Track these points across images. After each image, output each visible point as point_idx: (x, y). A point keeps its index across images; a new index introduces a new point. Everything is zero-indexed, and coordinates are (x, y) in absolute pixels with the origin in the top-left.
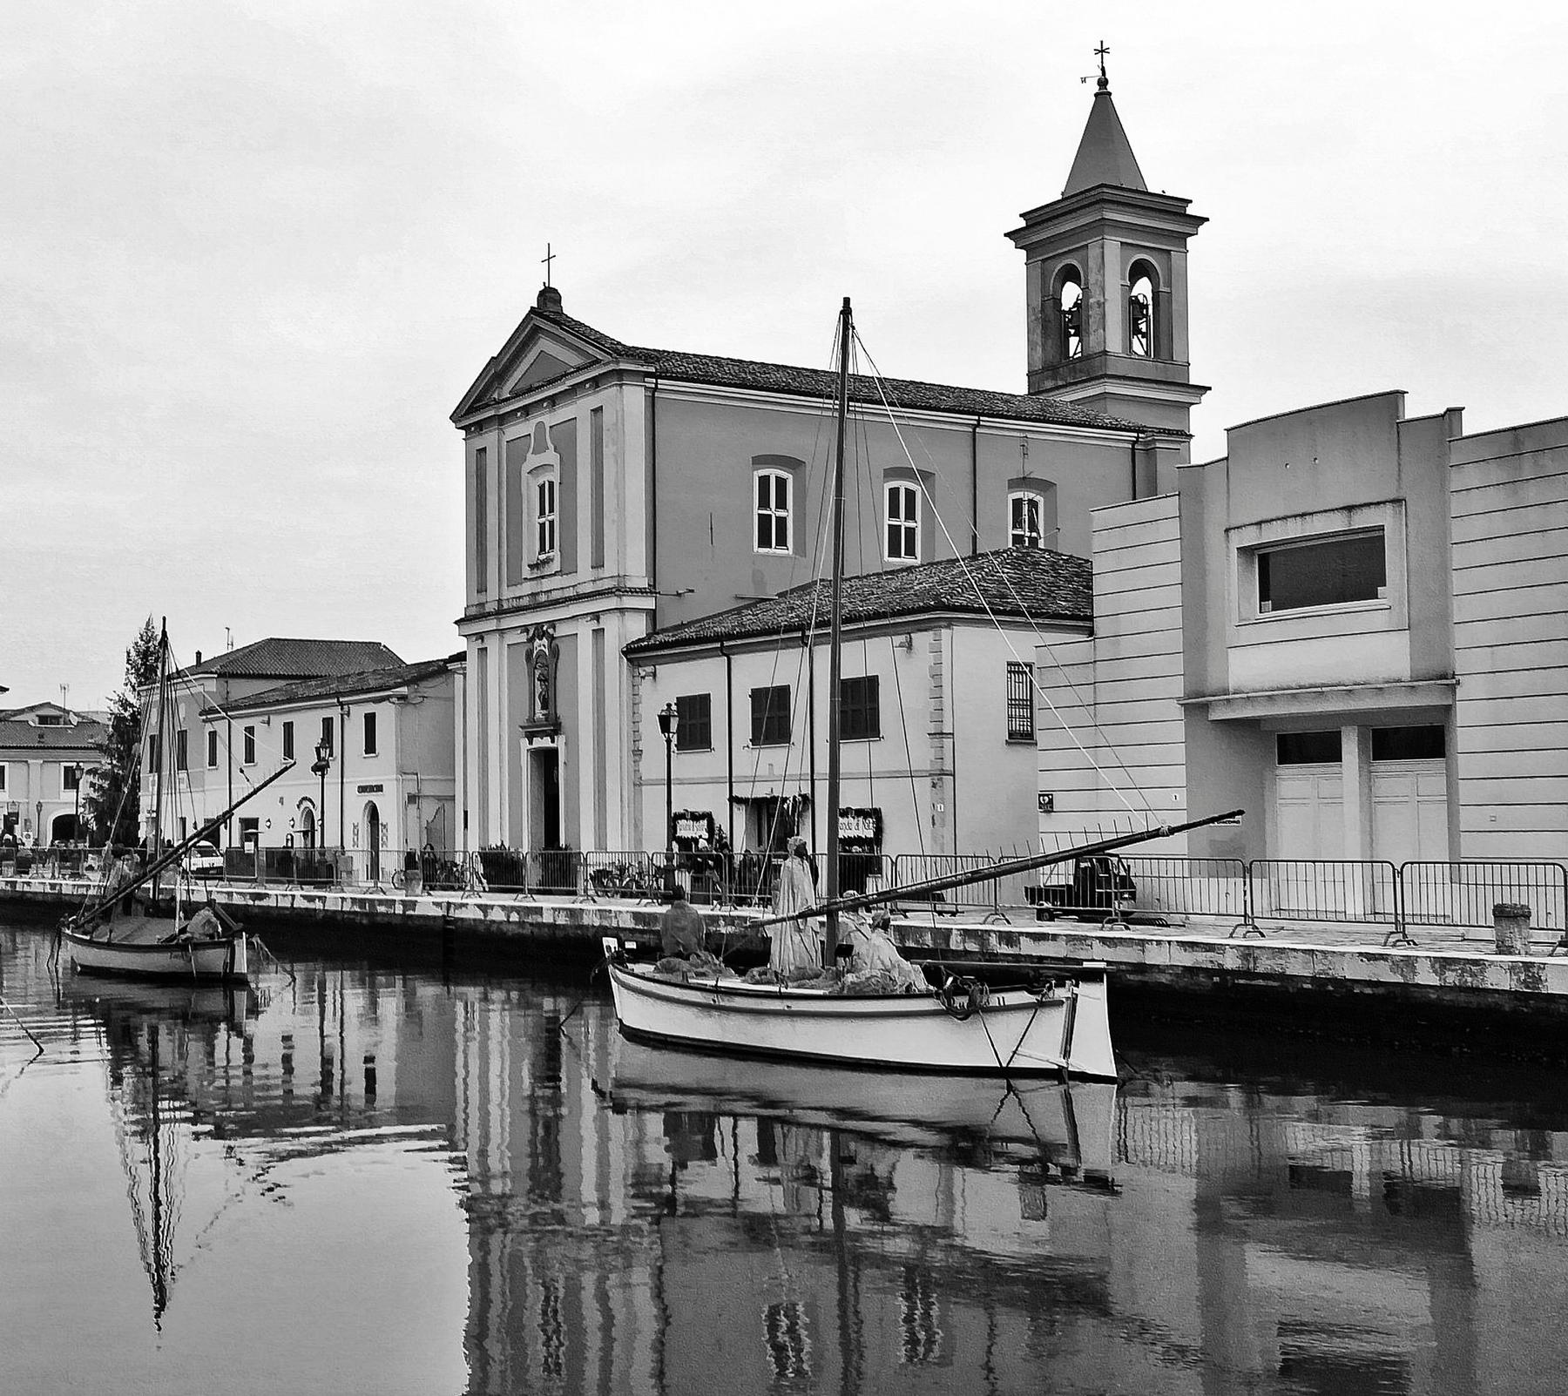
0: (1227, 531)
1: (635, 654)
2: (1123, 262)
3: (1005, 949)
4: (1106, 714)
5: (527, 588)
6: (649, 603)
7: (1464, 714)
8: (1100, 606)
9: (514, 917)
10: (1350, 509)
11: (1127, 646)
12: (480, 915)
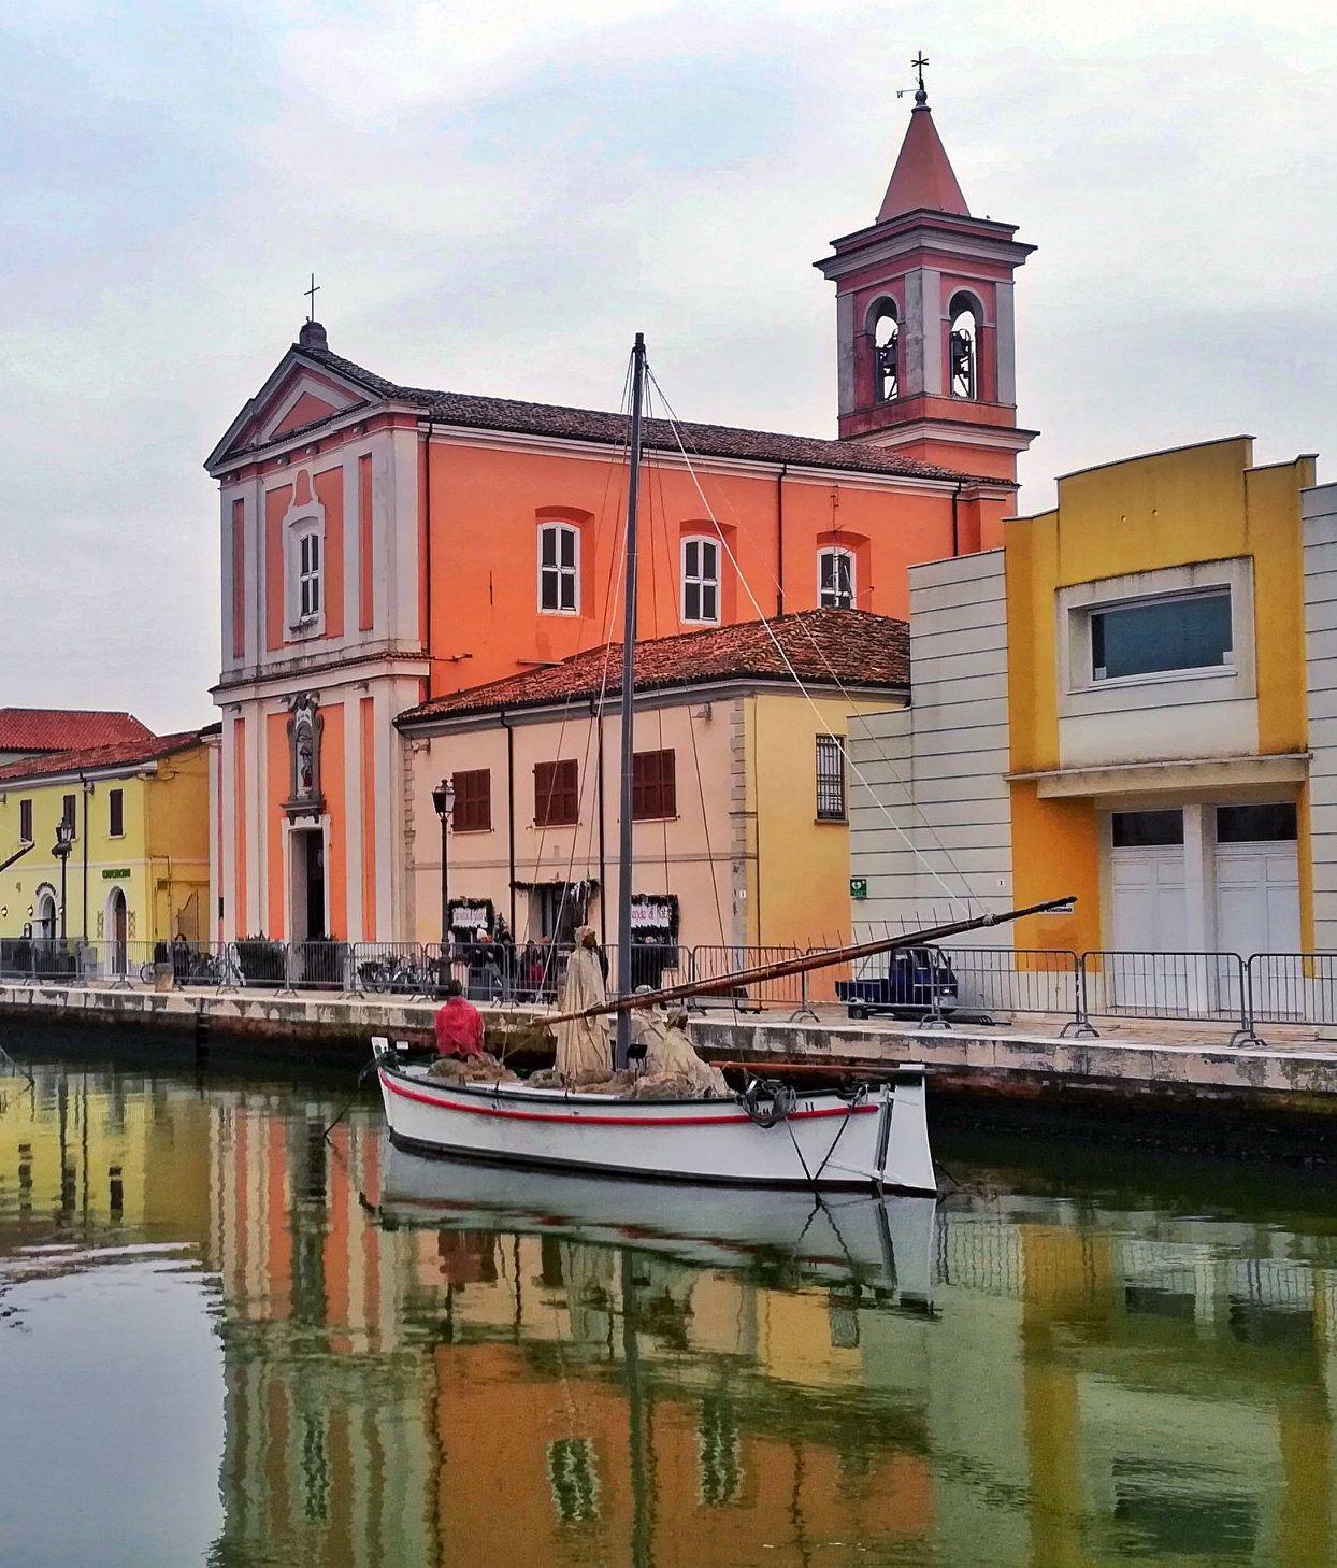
1: (406, 724)
3: (812, 1050)
4: (924, 790)
5: (288, 654)
6: (422, 669)
8: (917, 673)
9: (274, 1015)
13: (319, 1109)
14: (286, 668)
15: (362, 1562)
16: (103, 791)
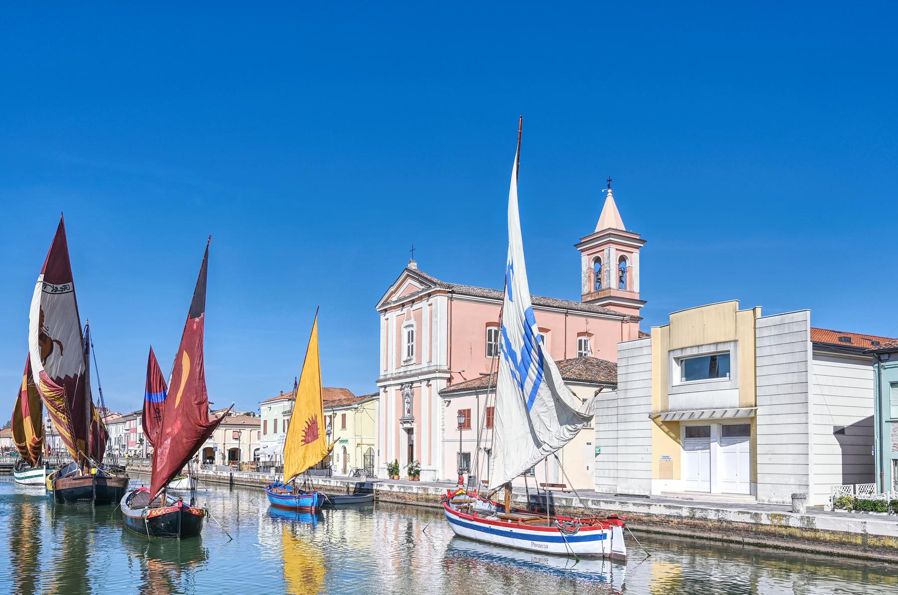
0: (670, 351)
1: (443, 393)
2: (617, 255)
3: (594, 507)
4: (622, 418)
5: (403, 369)
6: (448, 376)
7: (760, 420)
8: (620, 379)
9: (402, 490)
10: (717, 344)
11: (630, 394)
12: (389, 489)
13: (692, 563)
14: (401, 374)
15: (897, 567)
16: (339, 414)
